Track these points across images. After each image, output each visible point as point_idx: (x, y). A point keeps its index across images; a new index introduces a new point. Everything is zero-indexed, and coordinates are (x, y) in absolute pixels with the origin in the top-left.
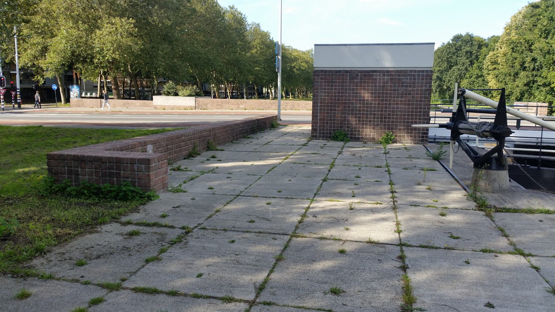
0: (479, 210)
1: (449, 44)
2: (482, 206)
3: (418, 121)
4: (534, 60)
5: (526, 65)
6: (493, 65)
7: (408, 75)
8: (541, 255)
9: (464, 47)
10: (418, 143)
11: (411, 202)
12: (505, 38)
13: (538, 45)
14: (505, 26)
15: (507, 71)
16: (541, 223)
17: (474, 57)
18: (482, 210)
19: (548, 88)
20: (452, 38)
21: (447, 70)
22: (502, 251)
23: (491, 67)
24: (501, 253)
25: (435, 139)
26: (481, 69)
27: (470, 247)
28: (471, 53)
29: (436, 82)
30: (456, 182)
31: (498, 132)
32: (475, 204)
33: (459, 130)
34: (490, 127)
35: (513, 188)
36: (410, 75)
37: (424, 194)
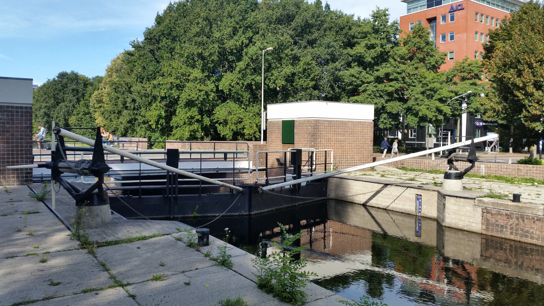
0: (82, 248)
1: (54, 80)
2: (85, 244)
3: (20, 160)
4: (134, 101)
5: (128, 105)
6: (99, 103)
7: (4, 111)
8: (138, 282)
9: (69, 85)
10: (22, 184)
11: (7, 254)
12: (108, 80)
13: (137, 87)
14: (107, 68)
15: (111, 108)
16: (139, 250)
17: (80, 95)
18: (85, 248)
19: (146, 125)
20: (57, 75)
21: (54, 106)
22: (103, 286)
23: (97, 105)
24: (101, 289)
25: (42, 178)
26: (87, 106)
27: (71, 291)
28: (77, 91)
29: (43, 118)
30: (60, 223)
31: (96, 168)
32: (78, 243)
33: (60, 169)
34: (88, 164)
35: (115, 220)
36: (6, 111)
37: (23, 241)
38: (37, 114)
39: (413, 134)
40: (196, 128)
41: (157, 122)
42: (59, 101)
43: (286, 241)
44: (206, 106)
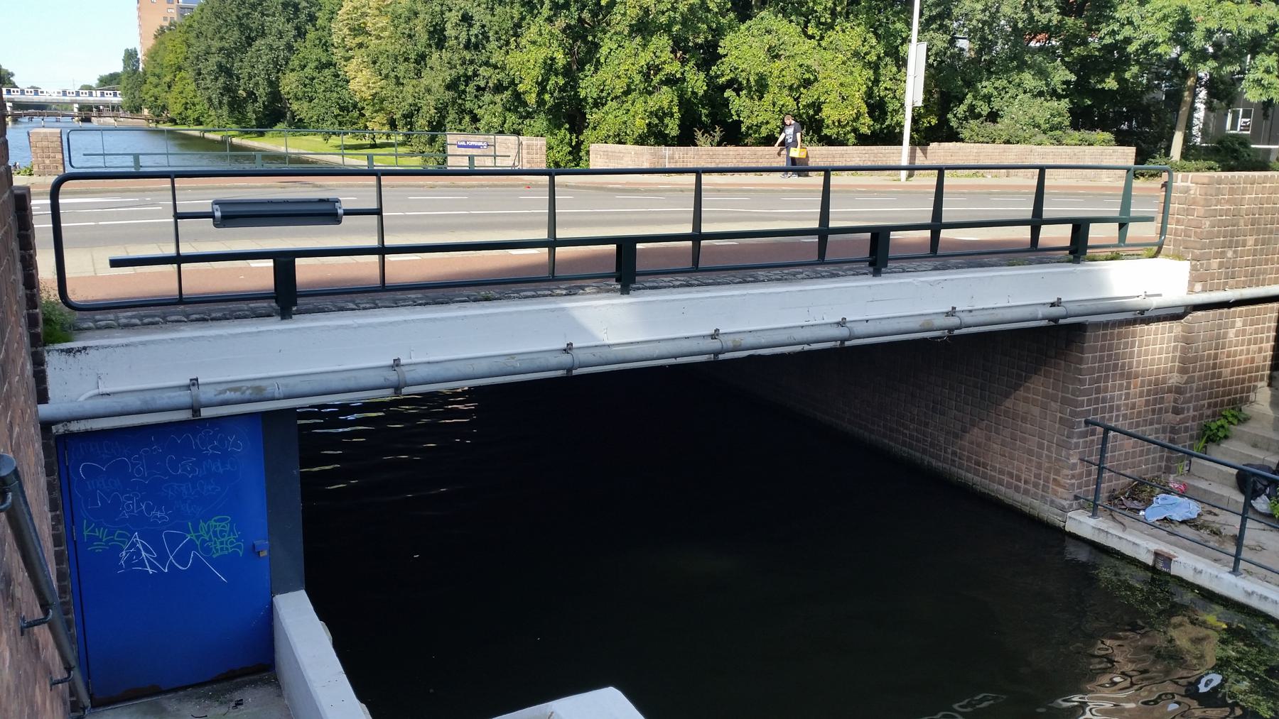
6: (355, 36)
17: (303, 17)
26: (326, 46)
29: (216, 79)
38: (200, 69)
39: (1241, 121)
40: (665, 104)
41: (542, 86)
42: (253, 35)
43: (239, 60)
44: (697, 33)
